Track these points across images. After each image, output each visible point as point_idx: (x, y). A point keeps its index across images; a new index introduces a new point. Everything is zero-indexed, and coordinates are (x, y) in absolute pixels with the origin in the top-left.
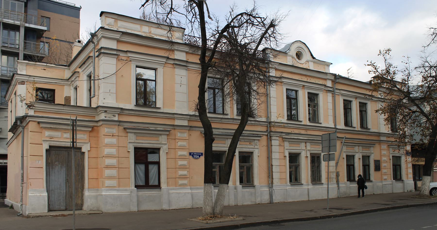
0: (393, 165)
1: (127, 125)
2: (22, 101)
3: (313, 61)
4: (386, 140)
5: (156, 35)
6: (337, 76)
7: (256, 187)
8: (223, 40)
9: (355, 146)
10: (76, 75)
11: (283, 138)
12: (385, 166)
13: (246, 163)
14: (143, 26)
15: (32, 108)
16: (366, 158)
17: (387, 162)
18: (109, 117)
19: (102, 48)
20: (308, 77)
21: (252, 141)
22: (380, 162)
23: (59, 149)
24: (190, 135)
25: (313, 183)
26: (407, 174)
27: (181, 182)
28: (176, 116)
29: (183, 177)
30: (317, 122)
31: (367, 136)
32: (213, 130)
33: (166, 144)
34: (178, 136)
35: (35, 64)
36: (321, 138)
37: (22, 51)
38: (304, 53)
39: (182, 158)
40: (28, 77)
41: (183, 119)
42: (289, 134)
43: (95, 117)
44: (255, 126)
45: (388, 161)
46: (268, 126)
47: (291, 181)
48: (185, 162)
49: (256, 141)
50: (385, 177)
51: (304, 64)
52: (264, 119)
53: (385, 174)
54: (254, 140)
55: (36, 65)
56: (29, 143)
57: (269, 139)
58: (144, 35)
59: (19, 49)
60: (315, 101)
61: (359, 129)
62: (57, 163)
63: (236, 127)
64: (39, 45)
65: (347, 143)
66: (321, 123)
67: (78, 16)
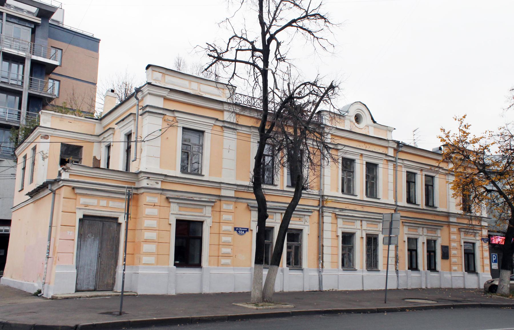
0: (465, 253)
1: (170, 194)
2: (44, 158)
3: (374, 126)
4: (456, 222)
5: (205, 93)
6: (401, 143)
7: (305, 270)
9: (419, 227)
10: (110, 132)
11: (336, 215)
12: (454, 254)
13: (294, 242)
14: (192, 83)
15: (67, 171)
16: (431, 244)
17: (457, 249)
18: (152, 184)
19: (147, 106)
20: (366, 145)
21: (302, 216)
22: (448, 248)
23: (94, 219)
24: (236, 207)
25: (368, 269)
26: (483, 266)
27: (223, 261)
28: (222, 185)
29: (227, 256)
30: (375, 196)
31: (432, 216)
33: (209, 217)
34: (224, 208)
35: (62, 116)
36: (382, 216)
37: (27, 90)
38: (363, 116)
39: (227, 233)
40: (54, 130)
41: (230, 189)
42: (343, 210)
43: (135, 183)
44: (306, 200)
45: (459, 248)
46: (321, 200)
47: (343, 265)
48: (228, 239)
49: (306, 217)
50: (455, 268)
51: (364, 129)
52: (316, 192)
53: (455, 264)
54: (305, 215)
55: (63, 117)
56: (61, 211)
57: (321, 216)
58: (192, 92)
59: (23, 86)
60: (373, 172)
61: (424, 207)
62: (90, 235)
63: (289, 200)
64: (47, 83)
65: (407, 222)
66: (379, 199)
67: (96, 50)
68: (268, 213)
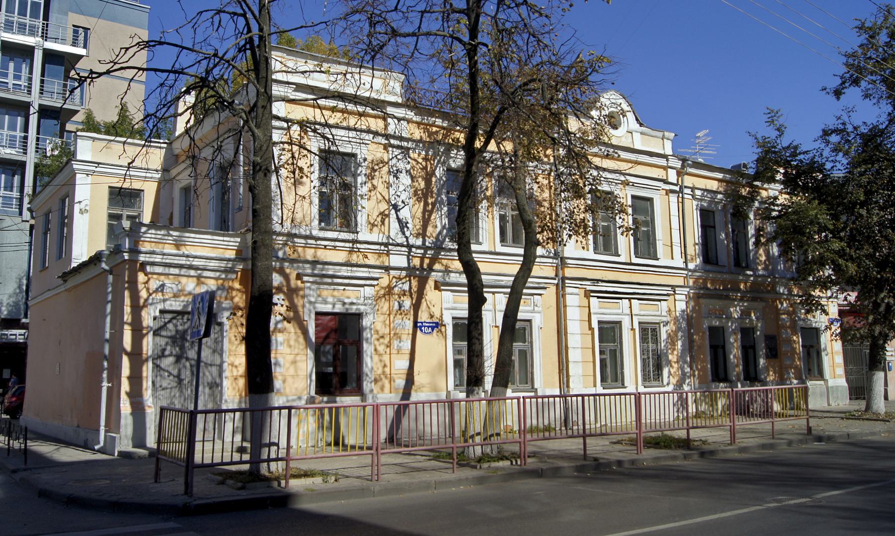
8: (378, 22)
32: (483, 277)
47: (603, 380)
63: (515, 269)
68: (486, 295)
